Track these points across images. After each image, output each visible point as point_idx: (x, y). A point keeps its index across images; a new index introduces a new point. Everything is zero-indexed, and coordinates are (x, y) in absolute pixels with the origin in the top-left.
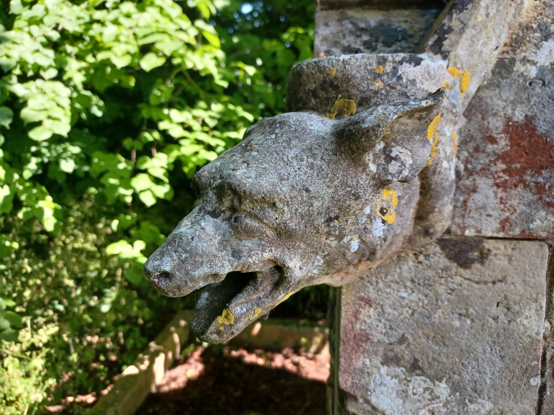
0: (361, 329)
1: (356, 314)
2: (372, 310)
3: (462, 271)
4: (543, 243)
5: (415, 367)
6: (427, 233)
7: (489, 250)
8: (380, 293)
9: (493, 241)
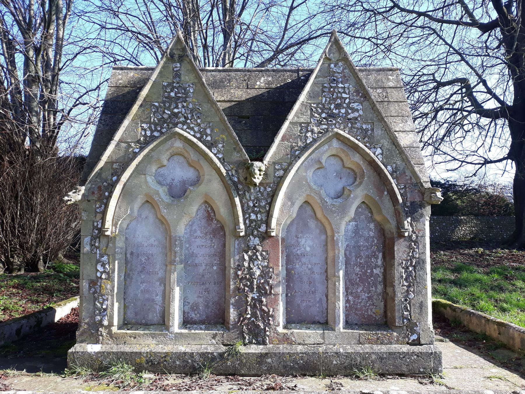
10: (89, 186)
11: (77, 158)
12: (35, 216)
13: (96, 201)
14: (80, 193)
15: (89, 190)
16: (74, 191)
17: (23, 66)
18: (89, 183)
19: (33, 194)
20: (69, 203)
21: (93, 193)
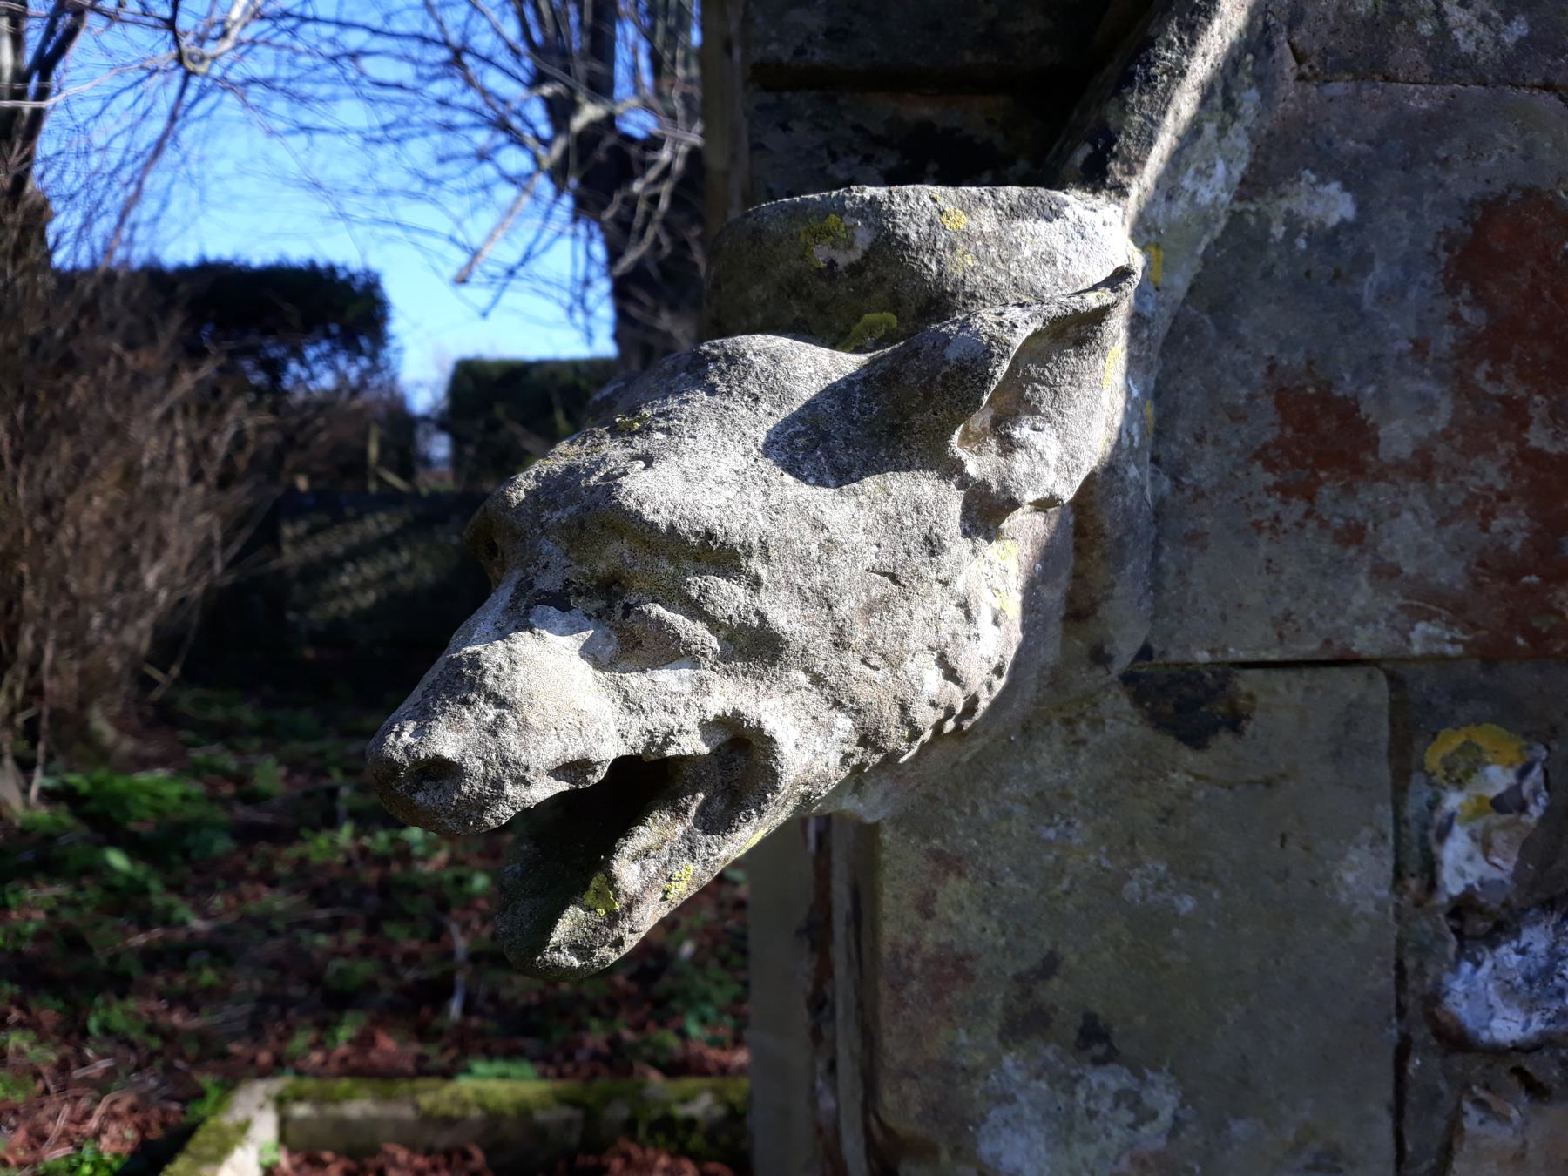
0: (939, 946)
1: (925, 907)
2: (964, 884)
3: (1189, 757)
4: (1376, 670)
5: (1094, 1038)
6: (1099, 656)
7: (1250, 697)
8: (984, 835)
9: (1258, 673)
13: (1416, 710)
21: (1320, 438)
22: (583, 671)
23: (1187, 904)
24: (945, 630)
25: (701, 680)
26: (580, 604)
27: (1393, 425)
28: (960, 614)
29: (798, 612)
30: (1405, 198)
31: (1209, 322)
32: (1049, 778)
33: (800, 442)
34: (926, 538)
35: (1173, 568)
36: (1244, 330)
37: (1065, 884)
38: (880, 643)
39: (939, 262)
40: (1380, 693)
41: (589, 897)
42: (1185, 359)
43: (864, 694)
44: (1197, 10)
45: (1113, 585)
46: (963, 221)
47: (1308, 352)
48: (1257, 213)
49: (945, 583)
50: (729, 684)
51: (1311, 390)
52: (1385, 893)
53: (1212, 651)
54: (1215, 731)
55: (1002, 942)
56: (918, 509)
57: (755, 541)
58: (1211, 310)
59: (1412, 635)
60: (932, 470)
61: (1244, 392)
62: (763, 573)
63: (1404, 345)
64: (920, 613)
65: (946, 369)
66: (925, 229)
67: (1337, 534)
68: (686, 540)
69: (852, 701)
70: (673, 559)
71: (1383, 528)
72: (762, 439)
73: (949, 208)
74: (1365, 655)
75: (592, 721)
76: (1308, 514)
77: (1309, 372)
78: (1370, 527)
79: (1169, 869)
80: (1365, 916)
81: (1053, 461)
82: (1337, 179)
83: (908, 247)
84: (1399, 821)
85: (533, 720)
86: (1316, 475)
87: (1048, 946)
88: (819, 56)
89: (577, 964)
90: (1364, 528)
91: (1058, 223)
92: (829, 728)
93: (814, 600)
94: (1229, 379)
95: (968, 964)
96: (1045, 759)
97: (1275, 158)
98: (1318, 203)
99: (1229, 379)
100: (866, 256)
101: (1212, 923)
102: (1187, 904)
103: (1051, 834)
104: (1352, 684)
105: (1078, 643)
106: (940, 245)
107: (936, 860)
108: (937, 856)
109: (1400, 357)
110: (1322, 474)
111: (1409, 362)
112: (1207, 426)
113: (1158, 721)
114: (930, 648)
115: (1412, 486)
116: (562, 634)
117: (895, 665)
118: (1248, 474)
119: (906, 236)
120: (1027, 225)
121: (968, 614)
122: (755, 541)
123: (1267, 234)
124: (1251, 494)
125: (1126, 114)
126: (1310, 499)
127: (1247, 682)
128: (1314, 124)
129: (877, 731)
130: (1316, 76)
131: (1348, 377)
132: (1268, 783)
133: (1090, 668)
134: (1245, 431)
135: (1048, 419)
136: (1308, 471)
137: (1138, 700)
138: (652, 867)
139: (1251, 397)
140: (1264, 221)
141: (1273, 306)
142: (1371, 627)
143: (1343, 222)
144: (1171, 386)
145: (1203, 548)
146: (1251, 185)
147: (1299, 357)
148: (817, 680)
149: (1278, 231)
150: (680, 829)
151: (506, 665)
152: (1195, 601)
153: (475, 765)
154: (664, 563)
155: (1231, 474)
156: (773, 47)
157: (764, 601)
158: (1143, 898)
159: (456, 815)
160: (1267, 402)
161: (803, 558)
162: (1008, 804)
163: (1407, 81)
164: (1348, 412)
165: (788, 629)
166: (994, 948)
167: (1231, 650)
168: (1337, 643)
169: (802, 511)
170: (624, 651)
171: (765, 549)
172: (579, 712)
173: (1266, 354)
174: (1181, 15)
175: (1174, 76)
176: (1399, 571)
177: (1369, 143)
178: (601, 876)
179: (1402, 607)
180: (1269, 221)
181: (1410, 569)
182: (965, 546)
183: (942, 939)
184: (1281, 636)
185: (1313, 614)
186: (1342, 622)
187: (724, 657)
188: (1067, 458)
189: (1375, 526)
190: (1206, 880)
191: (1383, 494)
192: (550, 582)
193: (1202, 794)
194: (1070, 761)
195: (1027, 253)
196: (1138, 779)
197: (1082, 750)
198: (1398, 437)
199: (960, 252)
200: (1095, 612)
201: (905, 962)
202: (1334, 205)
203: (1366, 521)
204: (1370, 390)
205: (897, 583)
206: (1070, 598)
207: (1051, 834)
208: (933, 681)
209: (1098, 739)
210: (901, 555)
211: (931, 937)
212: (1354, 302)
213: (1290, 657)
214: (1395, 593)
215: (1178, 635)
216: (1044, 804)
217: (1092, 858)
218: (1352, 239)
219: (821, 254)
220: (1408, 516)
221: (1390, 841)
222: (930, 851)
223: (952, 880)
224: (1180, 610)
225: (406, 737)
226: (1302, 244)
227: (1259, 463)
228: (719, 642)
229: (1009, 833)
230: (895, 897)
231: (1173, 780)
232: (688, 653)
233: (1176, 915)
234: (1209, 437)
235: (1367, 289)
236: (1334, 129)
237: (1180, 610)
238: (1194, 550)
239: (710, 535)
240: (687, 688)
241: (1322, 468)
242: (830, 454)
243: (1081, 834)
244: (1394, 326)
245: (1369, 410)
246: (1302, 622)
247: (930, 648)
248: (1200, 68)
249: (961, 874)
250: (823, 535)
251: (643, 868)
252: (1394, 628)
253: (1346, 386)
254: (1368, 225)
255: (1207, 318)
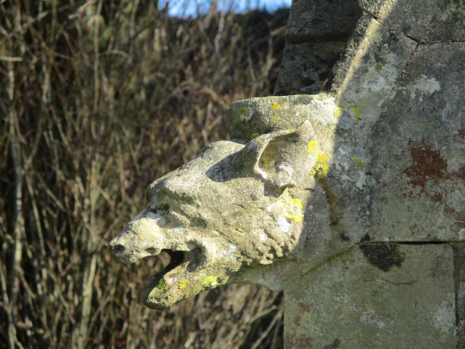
1: (297, 321)
3: (383, 274)
4: (447, 245)
10: (382, 83)
11: (239, 18)
12: (83, 266)
14: (287, 174)
15: (377, 131)
16: (228, 148)
17: (226, 155)
18: (375, 57)
19: (70, 168)
20: (177, 286)
22: (157, 228)
23: (381, 325)
24: (266, 223)
25: (186, 231)
26: (159, 212)
27: (453, 160)
28: (271, 218)
29: (211, 214)
30: (458, 82)
31: (389, 127)
32: (337, 280)
33: (216, 170)
34: (251, 196)
35: (376, 209)
36: (401, 130)
37: (342, 316)
38: (241, 225)
39: (270, 119)
40: (449, 253)
41: (160, 286)
42: (381, 140)
43: (238, 240)
44: (360, 35)
45: (342, 213)
46: (279, 107)
47: (423, 136)
48: (406, 90)
49: (263, 209)
50: (194, 233)
51: (424, 149)
52: (452, 325)
53: (390, 238)
54: (392, 266)
55: (321, 335)
56: (248, 188)
57: (197, 196)
58: (390, 124)
59: (459, 233)
60: (252, 177)
61: (400, 150)
62: (200, 203)
63: (456, 132)
64: (254, 217)
65: (248, 151)
66: (267, 110)
67: (432, 198)
68: (179, 195)
69: (234, 241)
70: (177, 200)
71: (449, 196)
72: (207, 169)
73: (275, 103)
74: (442, 240)
75: (156, 239)
76: (422, 191)
77: (423, 143)
78: (444, 195)
79: (376, 313)
80: (445, 333)
81: (291, 174)
82: (434, 77)
83: (261, 115)
84: (456, 299)
85: (142, 237)
86: (425, 178)
87: (336, 337)
88: (307, 31)
89: (157, 303)
90: (442, 195)
91: (309, 105)
92: (228, 248)
93: (215, 211)
94: (395, 146)
95: (310, 341)
96: (336, 274)
97: (413, 71)
98: (427, 86)
99: (395, 146)
100: (252, 118)
101: (390, 332)
102: (381, 325)
103: (338, 299)
104: (439, 250)
105: (336, 233)
106: (270, 114)
107: (301, 306)
108: (301, 305)
109: (455, 136)
110: (427, 177)
111: (458, 138)
112: (388, 162)
113: (372, 261)
114: (261, 227)
115: (459, 181)
116: (153, 219)
117: (248, 231)
118: (402, 178)
119: (261, 112)
120: (299, 106)
121: (274, 218)
122: (197, 196)
123: (409, 97)
124: (402, 184)
125: (337, 69)
126: (423, 186)
127: (402, 249)
128: (426, 59)
129: (245, 251)
130: (428, 42)
131: (436, 144)
132: (410, 284)
133: (342, 242)
134: (401, 163)
135: (289, 163)
136: (422, 177)
137: (366, 254)
138: (176, 279)
139: (403, 152)
140: (409, 93)
141: (411, 121)
142: (444, 230)
143: (436, 91)
144: (376, 149)
145: (386, 203)
146: (404, 79)
147: (420, 138)
148: (221, 234)
149: (413, 96)
150: (183, 271)
151: (137, 225)
152: (384, 221)
153: (127, 247)
154: (175, 201)
155: (396, 178)
156: (293, 29)
157: (200, 210)
158: (367, 322)
159: (123, 259)
160: (408, 153)
161: (211, 200)
162: (324, 288)
163: (460, 41)
164: (436, 156)
165: (207, 218)
166: (319, 336)
167: (396, 237)
168: (432, 236)
169: (211, 188)
170: (167, 223)
171: (200, 198)
172: (153, 237)
173: (408, 137)
174: (355, 37)
175: (352, 56)
176: (454, 211)
177: (446, 63)
178: (161, 280)
179: (456, 223)
180: (410, 92)
181: (458, 210)
182: (267, 199)
183: (302, 333)
184: (413, 233)
185: (424, 225)
186: (434, 228)
187: (191, 226)
188: (296, 173)
189: (446, 195)
190: (388, 316)
191: (448, 184)
192: (153, 207)
193: (387, 287)
194: (343, 274)
195: (297, 114)
196: (365, 281)
197: (347, 271)
198: (454, 164)
199: (276, 116)
200: (338, 223)
201: (291, 340)
202: (432, 85)
203: (442, 193)
204: (444, 148)
205: (243, 208)
206: (331, 218)
207: (338, 299)
208: (263, 237)
209: (353, 267)
210: (243, 200)
211: (299, 332)
212: (438, 118)
213: (416, 240)
214: (453, 218)
215: (378, 232)
216: (336, 288)
217: (350, 307)
218: (439, 97)
219: (242, 117)
220: (457, 191)
221: (454, 307)
222: (299, 303)
223: (306, 313)
224: (379, 224)
225: (115, 241)
226: (421, 99)
227: (405, 174)
228: (190, 221)
229: (324, 298)
230: (288, 318)
231: (377, 282)
232: (182, 224)
233: (378, 328)
234: (389, 166)
235: (443, 114)
236: (433, 60)
237: (379, 224)
238: (383, 204)
239: (184, 194)
240: (182, 233)
241: (427, 175)
242: (223, 173)
243: (346, 299)
244: (453, 126)
245: (443, 155)
246: (420, 228)
247: (261, 227)
248: (361, 52)
249: (308, 311)
250: (217, 194)
251: (173, 279)
252: (453, 230)
253: (436, 147)
254: (445, 92)
255: (388, 126)
